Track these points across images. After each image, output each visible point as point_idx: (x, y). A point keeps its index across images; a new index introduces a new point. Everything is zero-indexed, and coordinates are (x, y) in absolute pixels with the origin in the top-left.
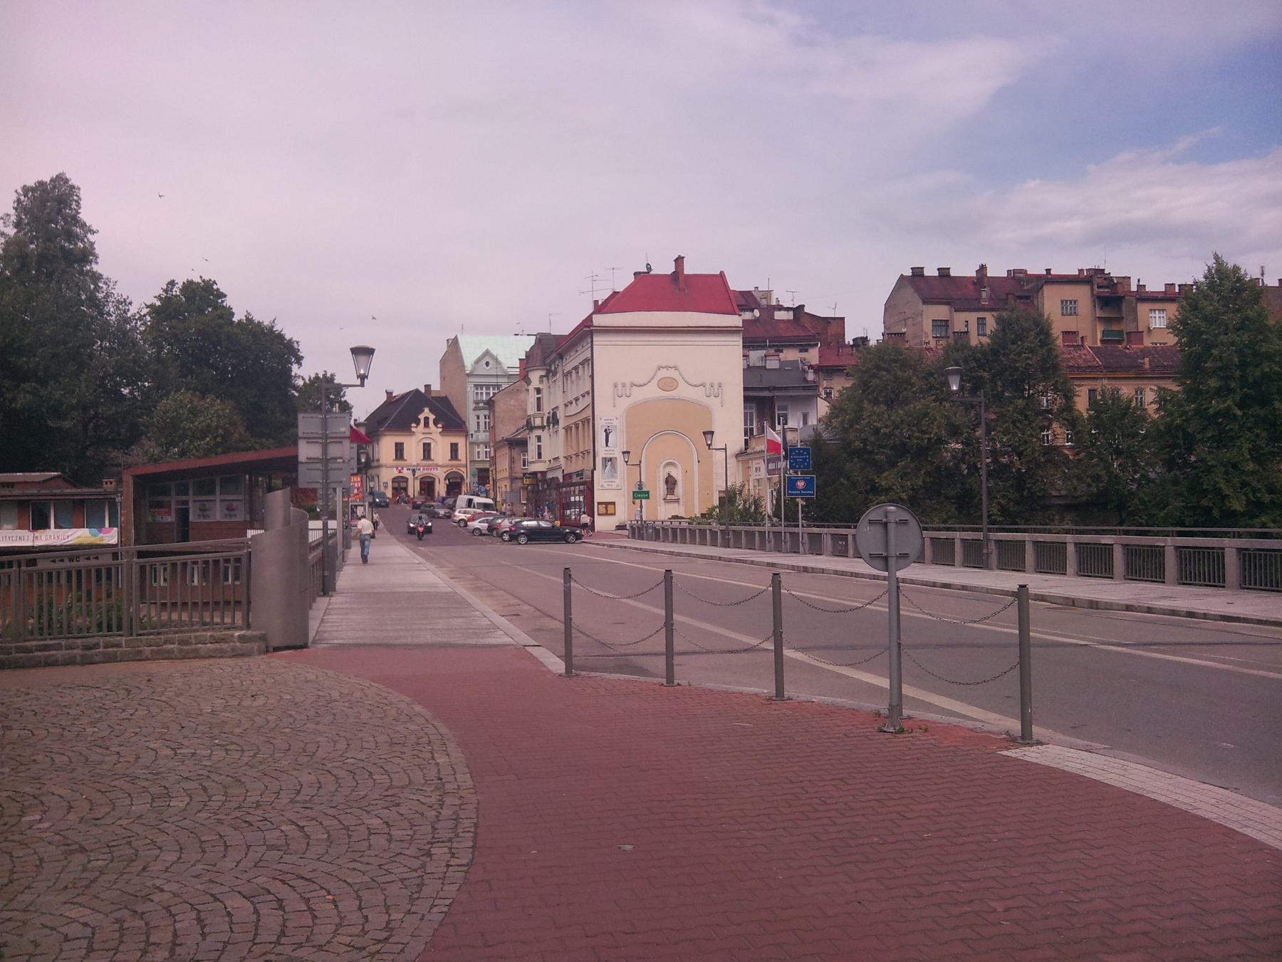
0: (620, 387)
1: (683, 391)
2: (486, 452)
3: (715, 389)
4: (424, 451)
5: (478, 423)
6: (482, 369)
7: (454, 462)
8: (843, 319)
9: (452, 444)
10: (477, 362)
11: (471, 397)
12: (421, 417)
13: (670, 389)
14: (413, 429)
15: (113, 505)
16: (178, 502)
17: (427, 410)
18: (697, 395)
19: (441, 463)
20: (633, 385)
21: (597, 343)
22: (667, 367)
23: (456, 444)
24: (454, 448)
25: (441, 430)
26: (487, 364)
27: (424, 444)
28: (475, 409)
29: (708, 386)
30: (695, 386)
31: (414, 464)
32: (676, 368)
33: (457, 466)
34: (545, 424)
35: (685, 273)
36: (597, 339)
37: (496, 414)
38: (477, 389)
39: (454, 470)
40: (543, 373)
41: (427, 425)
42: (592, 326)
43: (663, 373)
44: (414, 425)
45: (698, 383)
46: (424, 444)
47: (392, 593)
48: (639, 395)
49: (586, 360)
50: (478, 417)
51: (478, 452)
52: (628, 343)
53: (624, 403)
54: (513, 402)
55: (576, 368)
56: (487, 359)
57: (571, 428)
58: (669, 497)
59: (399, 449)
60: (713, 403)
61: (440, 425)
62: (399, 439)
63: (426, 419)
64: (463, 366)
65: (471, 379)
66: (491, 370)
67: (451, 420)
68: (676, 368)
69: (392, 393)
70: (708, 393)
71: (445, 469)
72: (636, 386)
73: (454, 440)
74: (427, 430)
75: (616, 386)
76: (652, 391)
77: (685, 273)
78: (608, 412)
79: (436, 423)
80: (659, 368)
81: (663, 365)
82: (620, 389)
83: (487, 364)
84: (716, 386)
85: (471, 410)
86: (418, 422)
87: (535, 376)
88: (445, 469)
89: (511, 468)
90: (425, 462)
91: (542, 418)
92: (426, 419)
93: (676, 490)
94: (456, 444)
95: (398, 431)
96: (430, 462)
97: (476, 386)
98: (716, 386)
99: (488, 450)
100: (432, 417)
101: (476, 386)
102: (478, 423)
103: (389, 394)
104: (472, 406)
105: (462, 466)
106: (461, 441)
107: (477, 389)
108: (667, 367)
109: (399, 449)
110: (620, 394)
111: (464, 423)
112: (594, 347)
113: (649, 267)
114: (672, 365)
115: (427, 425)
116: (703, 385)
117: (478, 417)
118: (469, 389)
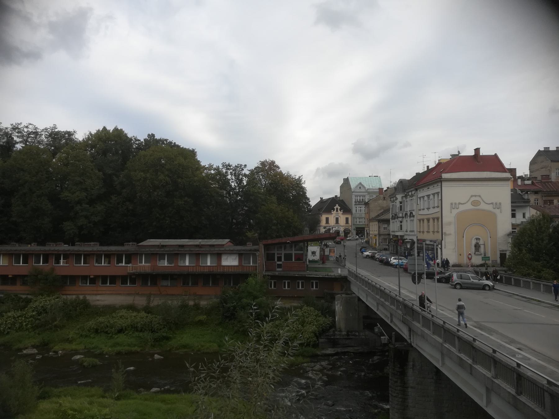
0: (454, 205)
1: (483, 206)
2: (359, 221)
3: (498, 206)
4: (336, 220)
5: (356, 210)
6: (358, 190)
7: (347, 225)
8: (515, 169)
9: (346, 218)
10: (356, 187)
11: (354, 200)
12: (335, 208)
13: (478, 205)
14: (332, 212)
15: (254, 255)
16: (278, 254)
17: (337, 205)
18: (489, 208)
19: (342, 225)
20: (460, 203)
21: (444, 186)
22: (475, 196)
23: (348, 218)
24: (347, 219)
25: (342, 213)
26: (360, 188)
27: (336, 218)
28: (355, 205)
29: (494, 204)
30: (489, 204)
31: (332, 225)
32: (479, 196)
33: (347, 226)
34: (404, 216)
35: (481, 154)
36: (444, 184)
37: (370, 208)
38: (356, 197)
39: (347, 227)
40: (404, 195)
41: (337, 211)
42: (442, 179)
43: (473, 199)
44: (332, 211)
45: (490, 203)
46: (336, 218)
47: (424, 331)
48: (462, 208)
49: (438, 193)
50: (356, 208)
51: (356, 221)
52: (462, 186)
53: (455, 212)
54: (376, 204)
55: (428, 196)
56: (360, 186)
57: (423, 220)
58: (477, 253)
59: (327, 219)
60: (497, 211)
61: (342, 211)
62: (327, 216)
63: (337, 208)
64: (351, 188)
65: (353, 194)
66: (363, 190)
67: (346, 209)
68: (479, 196)
69: (322, 198)
70: (494, 207)
71: (344, 227)
72: (461, 204)
73: (347, 216)
74: (337, 213)
75: (452, 204)
76: (469, 206)
77: (481, 154)
78: (449, 216)
79: (340, 210)
80: (472, 196)
81: (474, 195)
82: (454, 206)
83: (360, 188)
84: (498, 204)
85: (353, 206)
86: (334, 210)
87: (399, 197)
88: (344, 227)
89: (379, 230)
90: (336, 225)
91: (403, 214)
92: (337, 208)
93: (480, 250)
94: (348, 218)
95: (328, 213)
96: (338, 225)
97: (356, 196)
98: (498, 204)
99: (360, 220)
100: (339, 208)
101: (356, 196)
102: (356, 210)
103: (321, 199)
104: (354, 203)
105: (350, 226)
106: (349, 216)
107: (356, 197)
108: (475, 196)
109: (327, 219)
110: (454, 207)
111: (351, 210)
112: (443, 188)
113: (459, 152)
114: (478, 195)
115: (337, 211)
116: (492, 203)
117: (356, 208)
118: (353, 197)
